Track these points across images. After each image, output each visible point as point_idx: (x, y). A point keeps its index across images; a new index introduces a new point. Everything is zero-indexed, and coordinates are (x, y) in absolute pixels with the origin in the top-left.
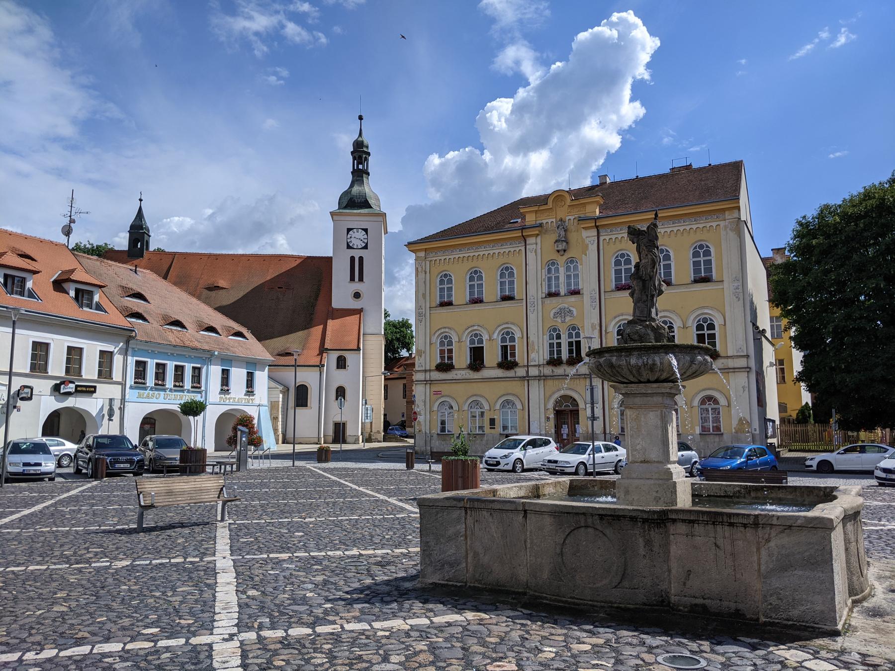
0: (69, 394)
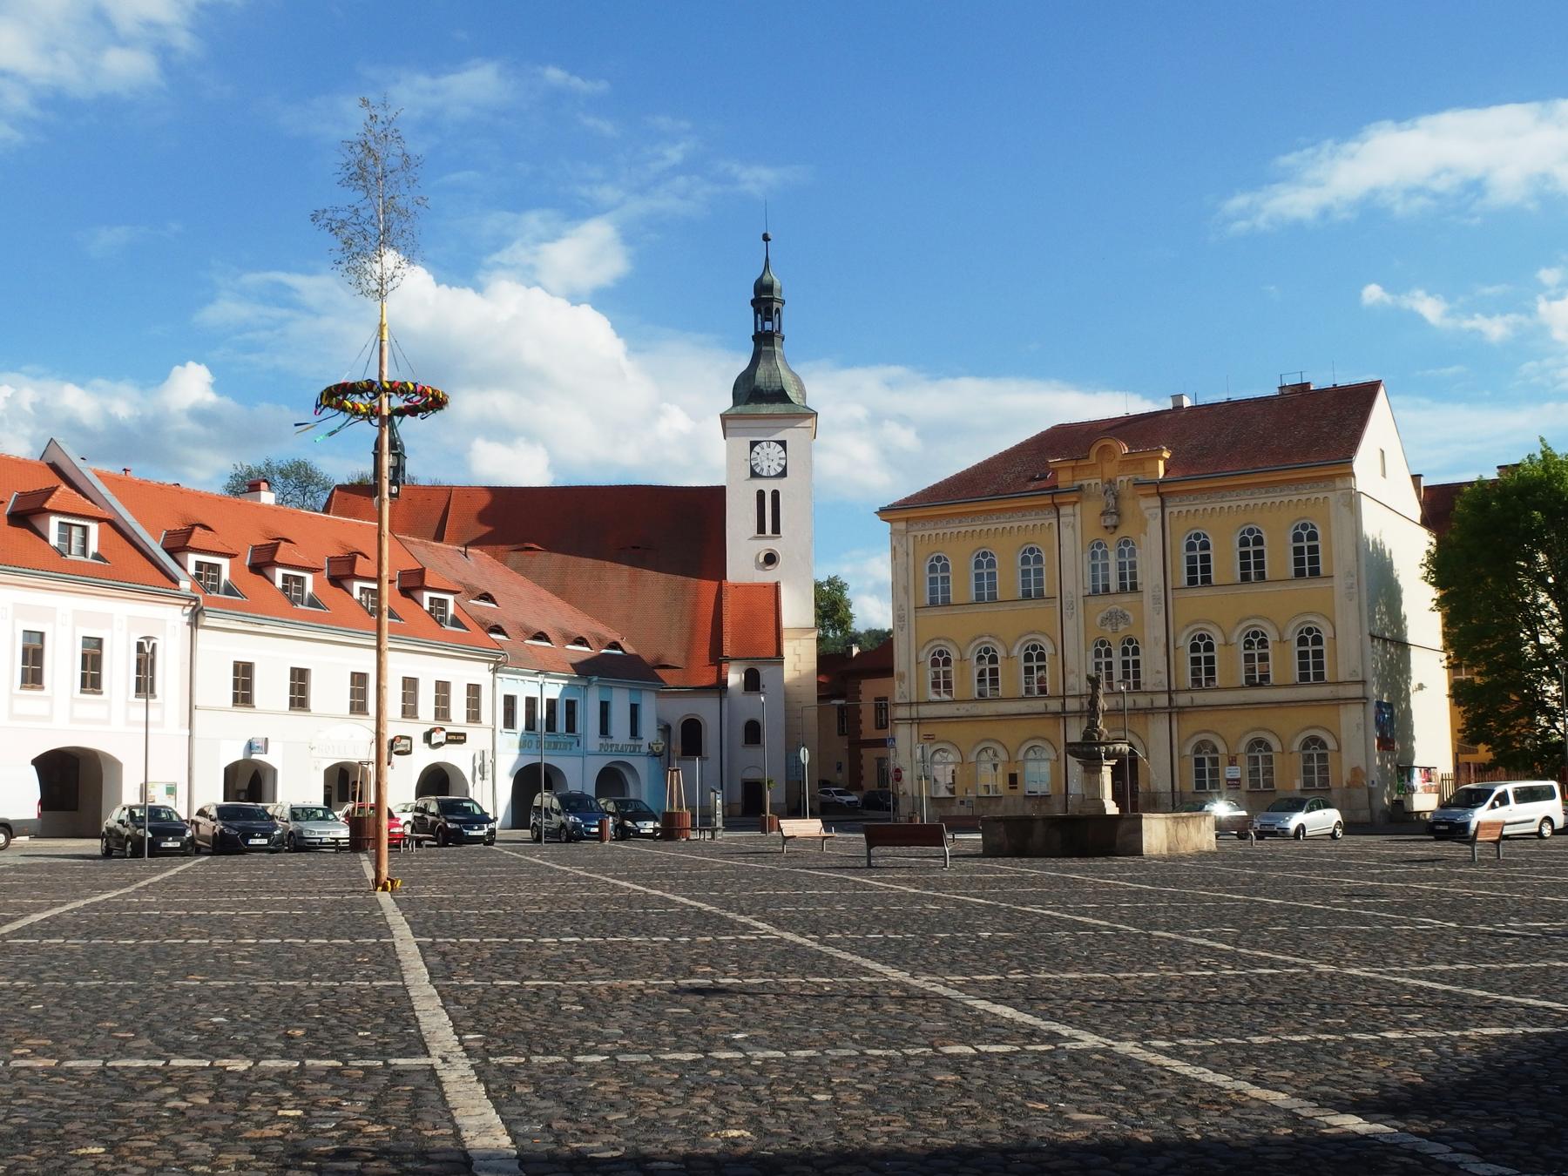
0: (440, 744)
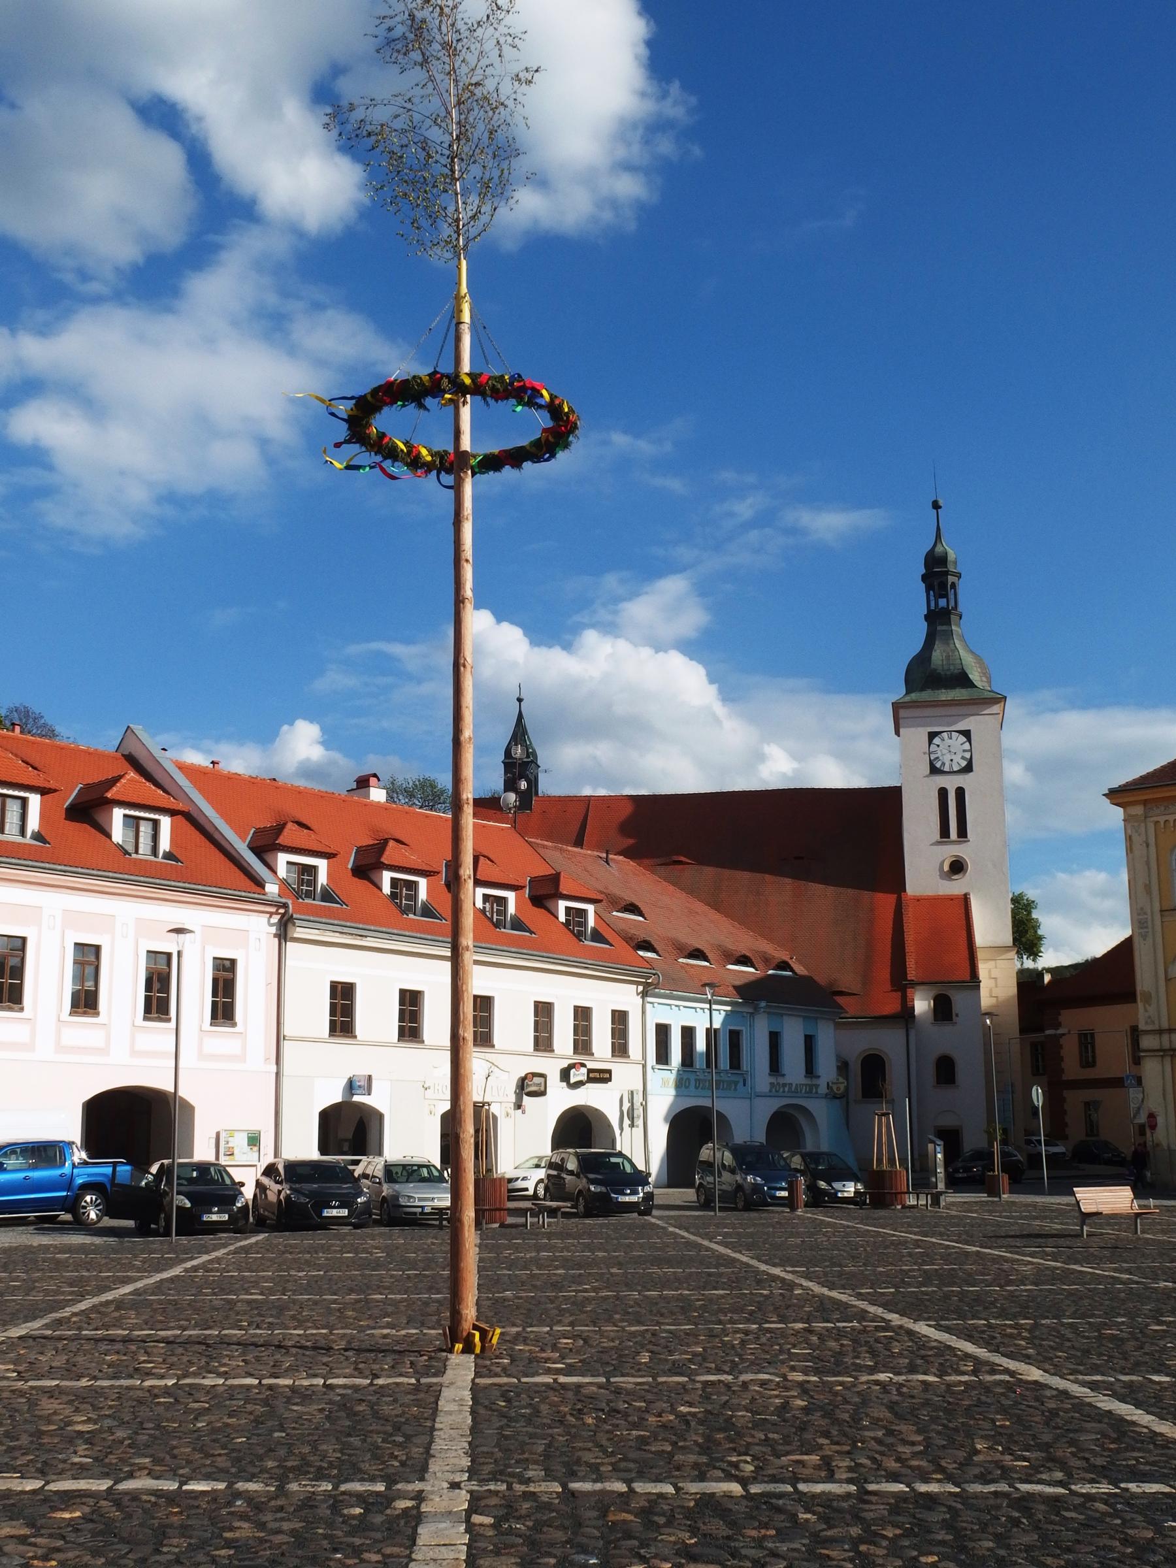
0: (579, 1084)
